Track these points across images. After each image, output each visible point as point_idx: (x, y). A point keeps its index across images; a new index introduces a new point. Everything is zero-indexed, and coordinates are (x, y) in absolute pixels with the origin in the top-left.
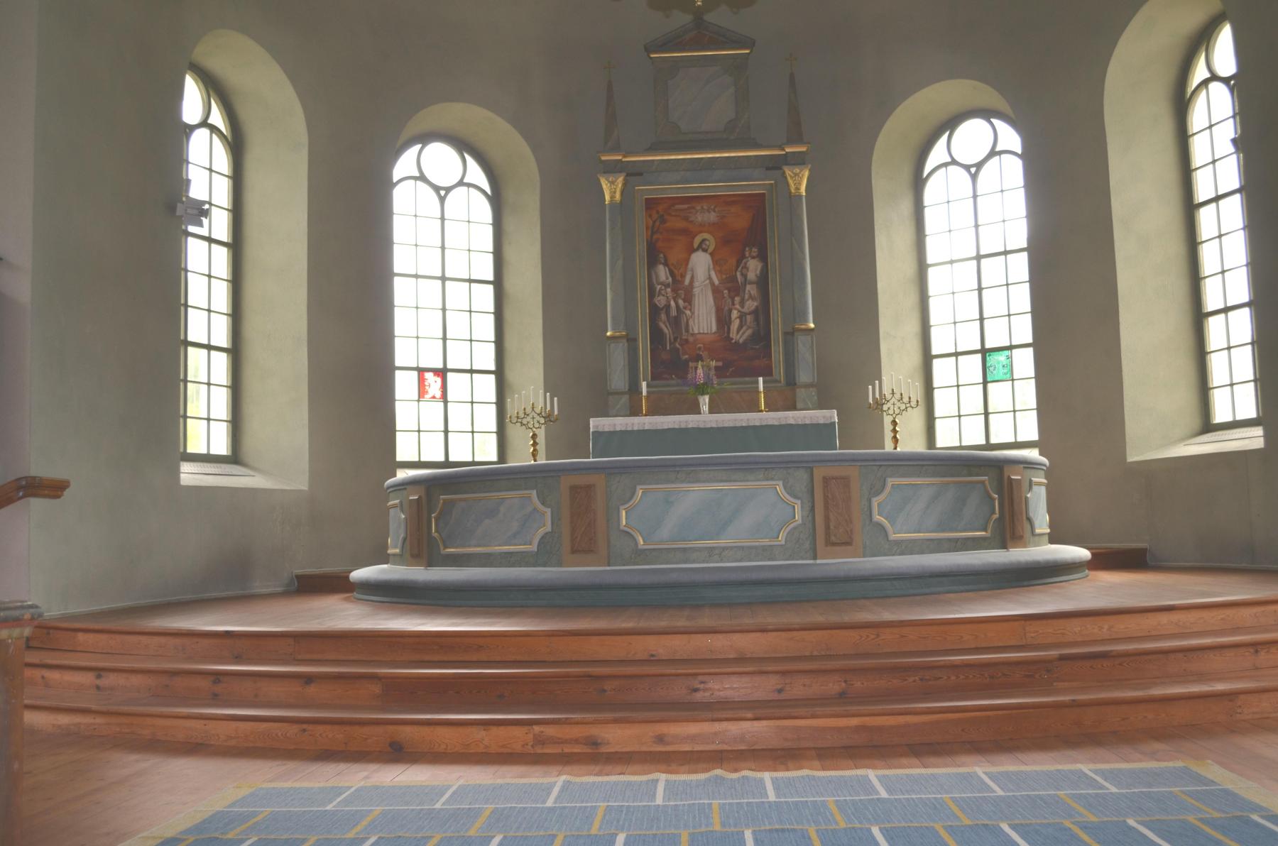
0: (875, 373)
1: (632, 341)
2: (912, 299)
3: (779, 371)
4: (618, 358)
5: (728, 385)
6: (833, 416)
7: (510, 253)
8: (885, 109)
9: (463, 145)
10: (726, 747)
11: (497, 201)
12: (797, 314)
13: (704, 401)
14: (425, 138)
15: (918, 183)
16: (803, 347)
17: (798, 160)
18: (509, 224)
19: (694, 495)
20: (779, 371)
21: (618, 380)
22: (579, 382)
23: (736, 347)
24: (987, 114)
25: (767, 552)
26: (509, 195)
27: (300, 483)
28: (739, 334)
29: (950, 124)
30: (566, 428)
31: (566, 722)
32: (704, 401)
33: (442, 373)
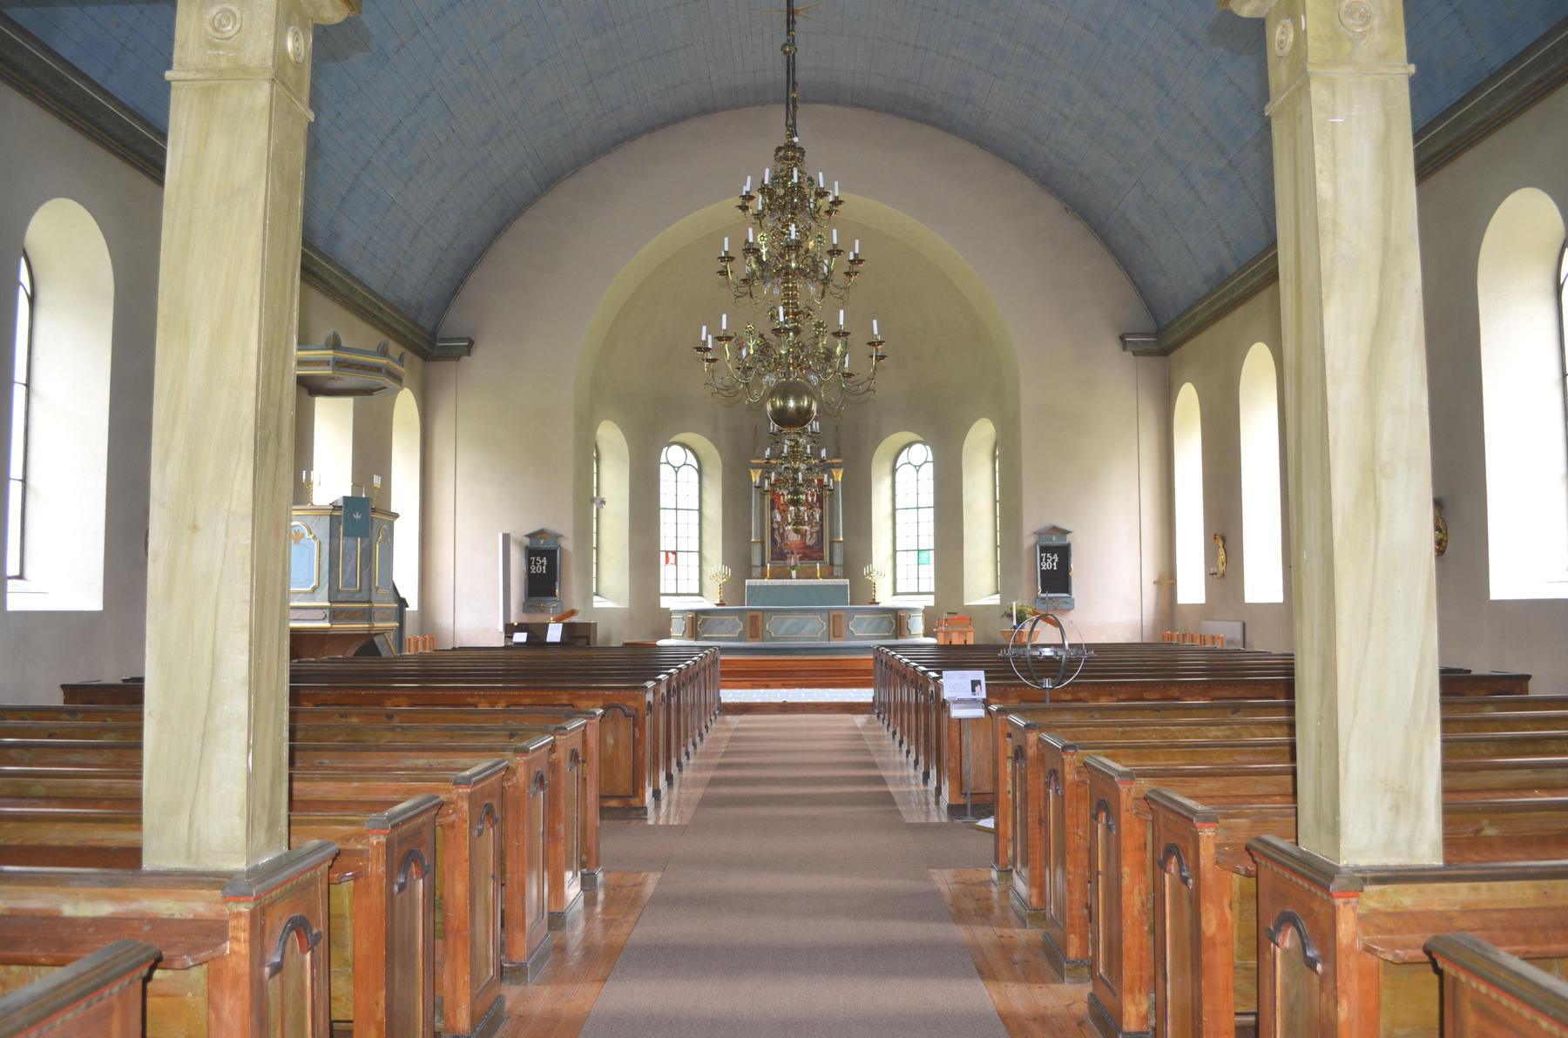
0: (870, 561)
1: (763, 543)
2: (890, 523)
3: (827, 559)
4: (756, 550)
5: (806, 564)
6: (847, 581)
7: (705, 496)
8: (878, 440)
9: (684, 446)
10: (307, 87)
11: (700, 471)
12: (833, 533)
13: (794, 573)
14: (669, 445)
15: (894, 471)
16: (838, 549)
17: (838, 466)
18: (706, 482)
19: (790, 620)
20: (827, 559)
21: (756, 561)
22: (740, 561)
23: (809, 547)
24: (924, 443)
25: (813, 639)
26: (706, 469)
27: (624, 604)
28: (810, 541)
29: (909, 445)
30: (734, 588)
31: (1506, 789)
32: (794, 573)
33: (675, 553)
